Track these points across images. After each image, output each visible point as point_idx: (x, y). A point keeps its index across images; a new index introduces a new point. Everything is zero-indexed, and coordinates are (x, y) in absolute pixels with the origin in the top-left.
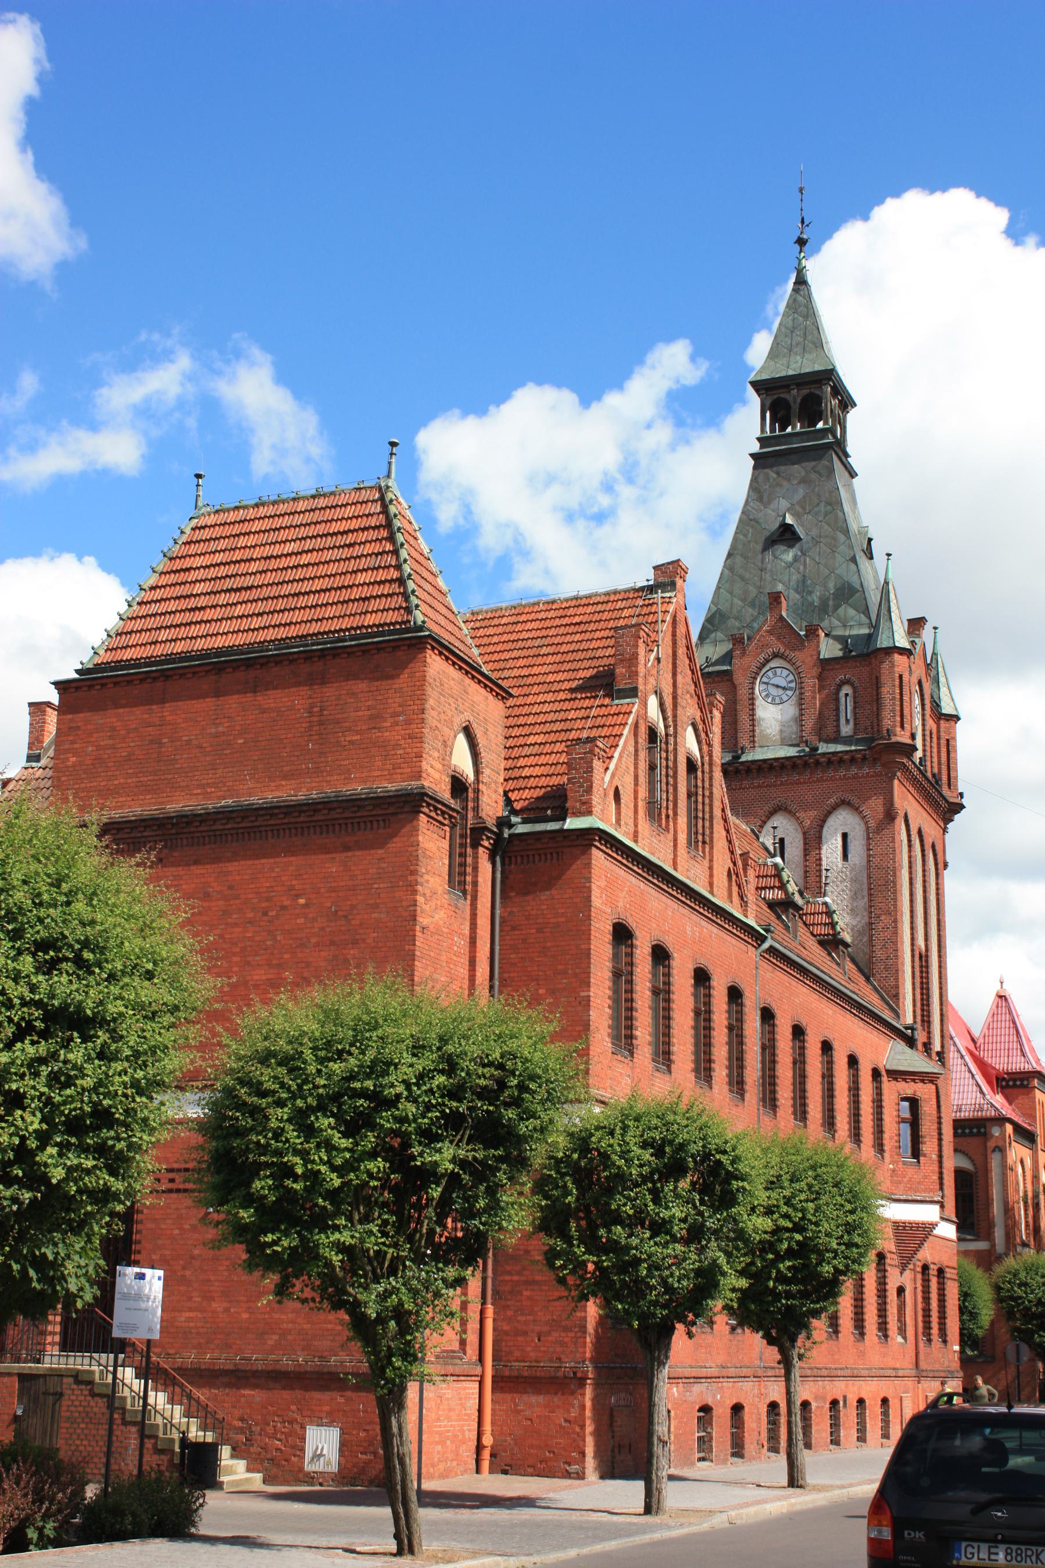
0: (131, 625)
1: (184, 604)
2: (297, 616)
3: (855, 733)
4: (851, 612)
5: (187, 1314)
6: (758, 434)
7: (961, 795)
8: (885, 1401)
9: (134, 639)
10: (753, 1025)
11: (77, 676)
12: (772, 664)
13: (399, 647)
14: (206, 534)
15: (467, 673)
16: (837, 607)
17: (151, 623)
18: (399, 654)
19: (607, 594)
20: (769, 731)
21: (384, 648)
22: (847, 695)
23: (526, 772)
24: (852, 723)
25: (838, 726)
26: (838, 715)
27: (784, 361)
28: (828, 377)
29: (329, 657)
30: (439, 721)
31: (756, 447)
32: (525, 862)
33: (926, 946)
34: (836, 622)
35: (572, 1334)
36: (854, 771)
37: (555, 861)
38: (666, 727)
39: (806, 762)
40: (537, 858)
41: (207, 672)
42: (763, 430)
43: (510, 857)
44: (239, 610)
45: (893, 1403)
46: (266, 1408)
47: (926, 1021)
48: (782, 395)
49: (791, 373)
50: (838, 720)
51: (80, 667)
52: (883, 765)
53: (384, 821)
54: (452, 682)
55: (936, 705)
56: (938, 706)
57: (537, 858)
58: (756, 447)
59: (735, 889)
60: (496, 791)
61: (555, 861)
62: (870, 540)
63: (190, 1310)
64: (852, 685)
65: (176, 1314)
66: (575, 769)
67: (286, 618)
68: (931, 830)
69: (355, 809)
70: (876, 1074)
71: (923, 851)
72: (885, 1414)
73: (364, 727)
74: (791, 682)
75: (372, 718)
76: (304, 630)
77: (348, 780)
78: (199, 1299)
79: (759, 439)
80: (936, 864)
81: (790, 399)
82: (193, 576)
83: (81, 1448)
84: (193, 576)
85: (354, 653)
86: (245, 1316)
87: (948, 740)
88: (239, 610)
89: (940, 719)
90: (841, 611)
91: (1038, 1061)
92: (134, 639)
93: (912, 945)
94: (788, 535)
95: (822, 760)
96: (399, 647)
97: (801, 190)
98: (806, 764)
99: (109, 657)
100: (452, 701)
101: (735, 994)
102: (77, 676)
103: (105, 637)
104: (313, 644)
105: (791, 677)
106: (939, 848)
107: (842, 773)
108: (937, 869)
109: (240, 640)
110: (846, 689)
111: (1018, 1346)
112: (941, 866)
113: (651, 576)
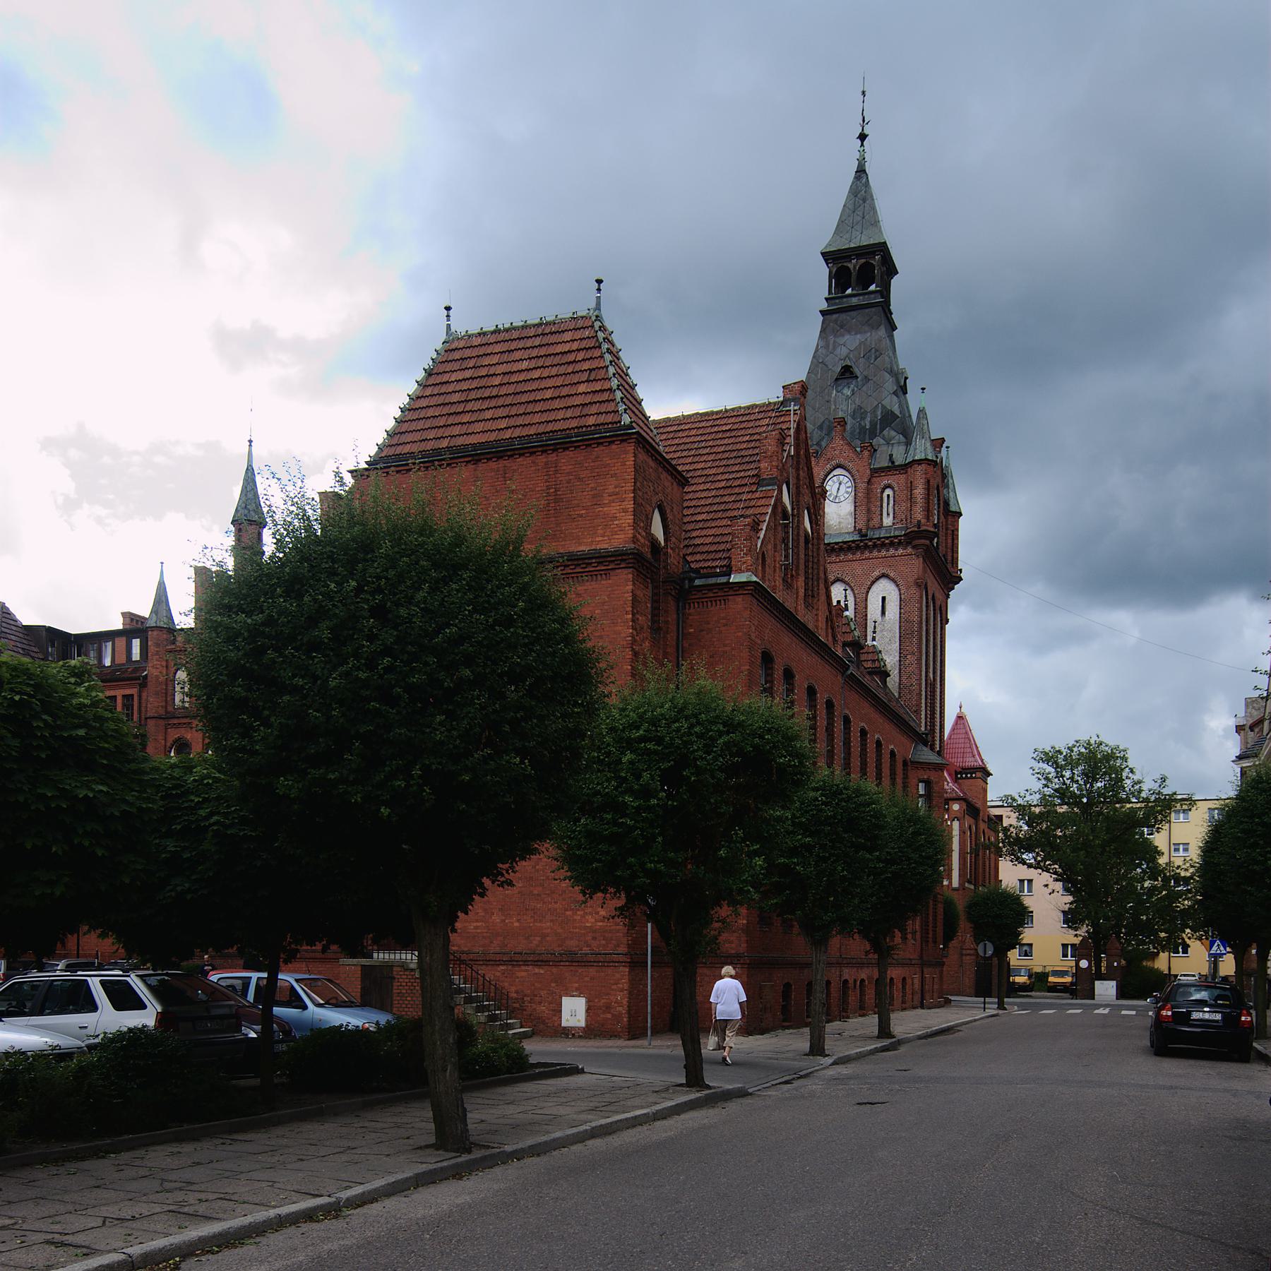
0: (405, 427)
1: (446, 410)
2: (537, 418)
3: (894, 524)
4: (893, 433)
5: (475, 924)
6: (826, 295)
7: (961, 570)
8: (904, 979)
9: (409, 438)
10: (839, 726)
11: (367, 466)
12: (835, 472)
13: (614, 441)
14: (457, 355)
15: (660, 463)
16: (882, 430)
17: (420, 425)
18: (614, 447)
19: (748, 408)
20: (831, 523)
21: (602, 443)
22: (888, 496)
23: (697, 541)
24: (891, 515)
25: (882, 519)
26: (882, 511)
27: (848, 236)
28: (882, 249)
29: (560, 451)
30: (643, 499)
31: (824, 306)
32: (701, 606)
33: (934, 677)
34: (882, 441)
35: (736, 934)
36: (892, 551)
37: (723, 606)
38: (793, 509)
39: (866, 544)
40: (709, 603)
41: (467, 462)
42: (830, 292)
43: (689, 603)
44: (488, 414)
45: (909, 981)
46: (534, 985)
47: (933, 730)
48: (845, 264)
49: (852, 245)
50: (882, 515)
51: (369, 459)
52: (914, 547)
53: (606, 574)
54: (651, 470)
55: (947, 504)
56: (949, 505)
57: (709, 603)
58: (824, 306)
59: (830, 631)
60: (679, 554)
61: (723, 606)
62: (906, 378)
63: (477, 921)
64: (893, 488)
65: (467, 924)
66: (738, 537)
67: (527, 420)
68: (939, 596)
69: (584, 566)
70: (905, 763)
71: (934, 610)
72: (904, 987)
73: (589, 504)
74: (848, 487)
75: (594, 496)
76: (541, 429)
77: (580, 544)
78: (483, 914)
79: (826, 299)
80: (941, 620)
81: (851, 266)
82: (451, 388)
83: (409, 1013)
84: (451, 388)
85: (579, 446)
86: (516, 924)
87: (953, 531)
88: (488, 414)
89: (948, 515)
90: (885, 432)
91: (982, 760)
92: (409, 438)
93: (926, 676)
94: (847, 375)
95: (870, 543)
96: (614, 441)
97: (863, 93)
98: (858, 547)
99: (391, 451)
100: (650, 484)
101: (830, 705)
102: (367, 466)
103: (386, 436)
104: (547, 441)
105: (849, 484)
106: (943, 609)
107: (884, 553)
108: (941, 624)
109: (492, 437)
110: (888, 492)
111: (985, 944)
112: (944, 621)
113: (781, 394)
